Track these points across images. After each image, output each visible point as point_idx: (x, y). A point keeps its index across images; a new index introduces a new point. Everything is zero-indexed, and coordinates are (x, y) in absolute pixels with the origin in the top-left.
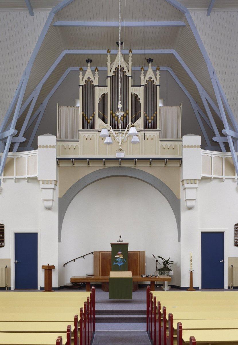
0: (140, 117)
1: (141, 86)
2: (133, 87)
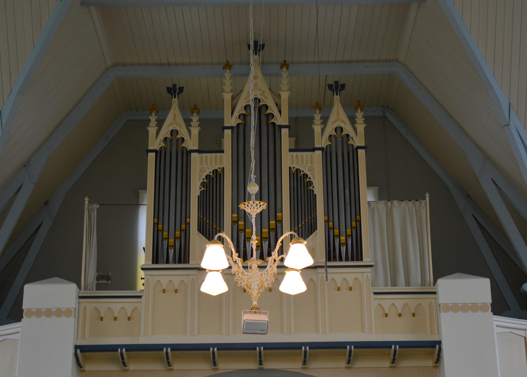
0: (316, 229)
1: (314, 150)
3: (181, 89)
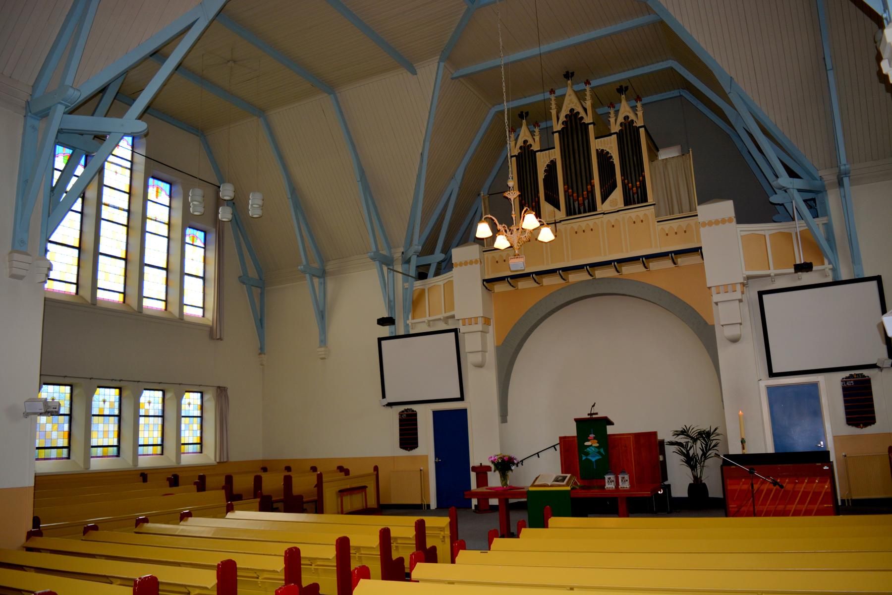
0: (616, 187)
1: (611, 135)
2: (599, 140)
3: (527, 113)
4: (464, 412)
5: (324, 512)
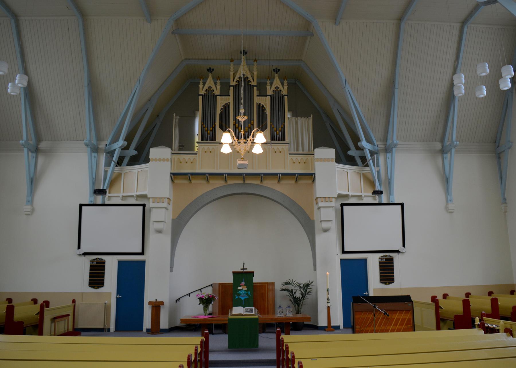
1: (267, 96)
3: (213, 70)
4: (143, 262)
5: (43, 334)
